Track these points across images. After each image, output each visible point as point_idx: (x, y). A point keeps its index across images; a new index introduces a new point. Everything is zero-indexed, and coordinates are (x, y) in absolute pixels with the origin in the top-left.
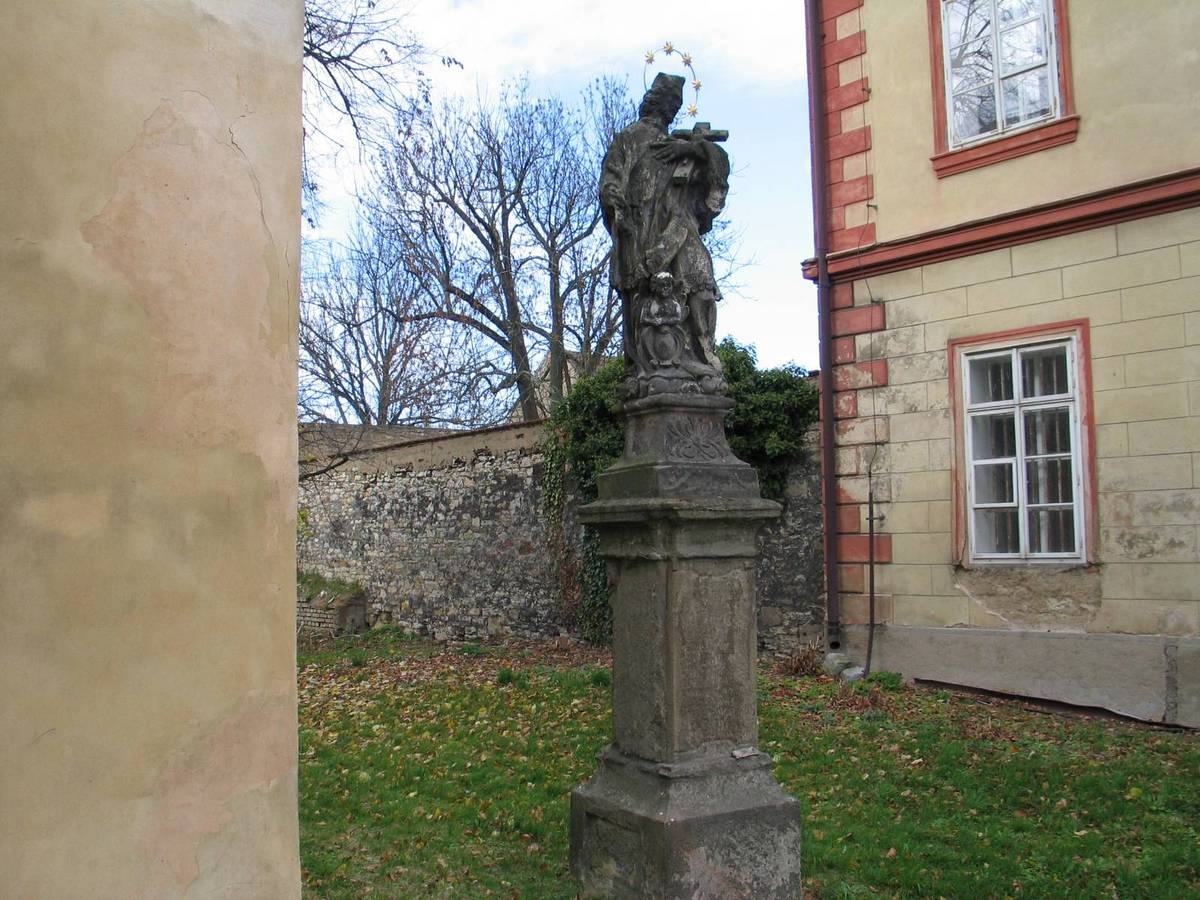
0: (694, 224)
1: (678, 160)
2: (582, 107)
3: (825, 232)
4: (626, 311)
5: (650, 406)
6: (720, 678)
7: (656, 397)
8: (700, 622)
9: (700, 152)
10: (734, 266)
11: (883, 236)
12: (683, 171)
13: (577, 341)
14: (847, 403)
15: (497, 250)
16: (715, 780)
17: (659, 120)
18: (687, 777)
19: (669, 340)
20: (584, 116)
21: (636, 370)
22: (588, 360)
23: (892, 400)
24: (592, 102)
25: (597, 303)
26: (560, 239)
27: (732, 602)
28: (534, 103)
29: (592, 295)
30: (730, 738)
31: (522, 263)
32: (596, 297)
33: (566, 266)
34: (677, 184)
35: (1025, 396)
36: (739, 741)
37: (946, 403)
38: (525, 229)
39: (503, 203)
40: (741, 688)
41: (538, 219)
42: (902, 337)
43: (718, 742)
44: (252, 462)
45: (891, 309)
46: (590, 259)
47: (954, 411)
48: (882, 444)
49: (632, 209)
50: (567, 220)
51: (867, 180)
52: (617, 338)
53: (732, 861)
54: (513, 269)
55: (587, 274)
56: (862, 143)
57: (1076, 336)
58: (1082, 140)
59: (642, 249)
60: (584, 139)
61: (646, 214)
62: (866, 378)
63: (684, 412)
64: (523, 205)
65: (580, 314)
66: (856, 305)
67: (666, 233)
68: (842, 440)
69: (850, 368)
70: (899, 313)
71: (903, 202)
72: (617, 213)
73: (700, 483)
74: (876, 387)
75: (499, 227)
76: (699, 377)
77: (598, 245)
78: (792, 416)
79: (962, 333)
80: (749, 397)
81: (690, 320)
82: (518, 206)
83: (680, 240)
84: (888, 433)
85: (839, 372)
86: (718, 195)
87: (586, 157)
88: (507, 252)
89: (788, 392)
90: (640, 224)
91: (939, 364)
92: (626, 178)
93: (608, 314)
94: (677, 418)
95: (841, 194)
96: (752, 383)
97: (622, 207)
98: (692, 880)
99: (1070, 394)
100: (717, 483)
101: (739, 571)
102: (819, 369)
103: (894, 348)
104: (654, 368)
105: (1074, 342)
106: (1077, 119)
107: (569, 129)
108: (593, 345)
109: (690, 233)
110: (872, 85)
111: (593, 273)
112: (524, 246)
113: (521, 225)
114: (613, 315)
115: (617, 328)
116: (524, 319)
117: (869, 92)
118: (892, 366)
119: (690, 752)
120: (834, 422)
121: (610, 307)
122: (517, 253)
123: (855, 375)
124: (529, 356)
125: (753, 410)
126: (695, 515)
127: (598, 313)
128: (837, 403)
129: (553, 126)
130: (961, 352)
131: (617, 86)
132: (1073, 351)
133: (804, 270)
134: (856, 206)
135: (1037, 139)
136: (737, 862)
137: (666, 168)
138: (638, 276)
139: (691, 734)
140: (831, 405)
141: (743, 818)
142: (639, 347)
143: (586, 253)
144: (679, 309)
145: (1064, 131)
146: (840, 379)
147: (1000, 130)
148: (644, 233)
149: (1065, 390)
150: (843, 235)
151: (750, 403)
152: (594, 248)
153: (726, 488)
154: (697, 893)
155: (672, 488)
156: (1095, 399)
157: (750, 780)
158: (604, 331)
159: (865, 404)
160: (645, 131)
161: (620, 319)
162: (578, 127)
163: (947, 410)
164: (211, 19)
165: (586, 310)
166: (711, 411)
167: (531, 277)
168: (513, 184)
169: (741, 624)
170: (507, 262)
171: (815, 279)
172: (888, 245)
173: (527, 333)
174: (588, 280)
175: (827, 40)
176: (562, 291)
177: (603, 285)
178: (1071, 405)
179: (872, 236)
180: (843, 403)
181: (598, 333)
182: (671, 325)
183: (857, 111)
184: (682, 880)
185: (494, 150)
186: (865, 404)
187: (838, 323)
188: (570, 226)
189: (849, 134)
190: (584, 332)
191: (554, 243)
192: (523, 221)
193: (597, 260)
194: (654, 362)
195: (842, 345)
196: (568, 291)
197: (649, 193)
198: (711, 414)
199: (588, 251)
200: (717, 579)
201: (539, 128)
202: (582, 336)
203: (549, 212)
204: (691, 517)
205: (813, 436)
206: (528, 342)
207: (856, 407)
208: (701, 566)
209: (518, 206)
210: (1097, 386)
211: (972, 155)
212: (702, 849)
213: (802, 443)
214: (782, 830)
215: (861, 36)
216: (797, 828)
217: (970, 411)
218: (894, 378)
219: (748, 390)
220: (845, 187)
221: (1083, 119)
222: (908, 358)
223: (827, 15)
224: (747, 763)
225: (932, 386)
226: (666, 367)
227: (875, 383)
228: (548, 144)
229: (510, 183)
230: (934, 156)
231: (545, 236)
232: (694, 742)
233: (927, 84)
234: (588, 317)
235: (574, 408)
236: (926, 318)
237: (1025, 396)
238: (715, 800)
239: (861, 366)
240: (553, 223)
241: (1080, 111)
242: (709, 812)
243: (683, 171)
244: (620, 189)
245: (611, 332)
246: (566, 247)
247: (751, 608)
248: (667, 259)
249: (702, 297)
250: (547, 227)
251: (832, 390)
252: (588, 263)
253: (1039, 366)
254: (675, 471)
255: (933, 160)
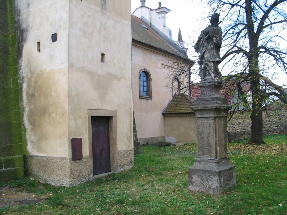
6: (206, 142)
8: (202, 130)
16: (203, 163)
18: (197, 161)
27: (209, 127)
30: (209, 155)
36: (211, 156)
40: (211, 145)
43: (206, 155)
44: (65, 109)
53: (202, 179)
63: (204, 87)
73: (202, 102)
98: (194, 181)
100: (206, 102)
101: (211, 120)
119: (201, 156)
126: (197, 109)
136: (203, 180)
139: (200, 153)
141: (205, 171)
153: (208, 102)
154: (195, 183)
155: (196, 104)
157: (211, 164)
169: (211, 131)
184: (192, 180)
198: (210, 87)
200: (206, 122)
204: (196, 109)
208: (202, 119)
212: (196, 175)
214: (214, 176)
216: (218, 177)
224: (210, 161)
232: (201, 155)
238: (202, 167)
242: (198, 168)
247: (214, 128)
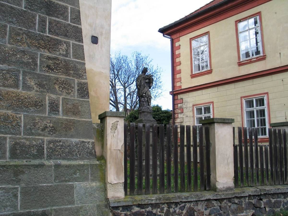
0: (148, 88)
1: (146, 79)
2: (131, 57)
3: (173, 87)
4: (139, 100)
5: (142, 112)
7: (143, 111)
9: (149, 78)
10: (163, 91)
11: (183, 87)
12: (147, 81)
13: (129, 106)
14: (177, 115)
15: (113, 87)
17: (144, 74)
19: (145, 103)
20: (132, 59)
21: (141, 107)
22: (132, 109)
23: (184, 115)
24: (133, 56)
25: (134, 98)
26: (126, 85)
28: (122, 56)
29: (133, 96)
31: (118, 90)
32: (134, 97)
33: (127, 90)
34: (146, 83)
35: (204, 114)
37: (192, 115)
38: (119, 83)
39: (115, 77)
41: (122, 80)
42: (186, 104)
45: (184, 99)
46: (132, 89)
47: (193, 116)
48: (182, 122)
49: (140, 86)
50: (128, 81)
51: (180, 78)
52: (138, 105)
54: (116, 91)
55: (132, 92)
56: (180, 72)
57: (212, 104)
58: (213, 73)
59: (141, 91)
60: (132, 64)
61: (142, 87)
62: (180, 111)
64: (119, 78)
65: (130, 100)
66: (178, 99)
67: (145, 89)
68: (176, 122)
69: (177, 110)
70: (185, 100)
71: (186, 82)
72: (138, 87)
73: (149, 122)
74: (181, 113)
75: (114, 82)
76: (149, 108)
77: (134, 87)
78: (168, 118)
79: (195, 104)
80: (160, 115)
81: (148, 101)
82: (118, 78)
83: (146, 90)
84: (183, 120)
85: (175, 110)
86: (152, 84)
87: (132, 68)
88: (115, 87)
89: (167, 114)
90: (141, 88)
91: (191, 109)
92: (139, 82)
93: (136, 101)
94: (145, 113)
95: (176, 80)
96: (161, 112)
97: (139, 86)
99: (211, 114)
102: (172, 110)
103: (184, 106)
104: (143, 107)
105: (211, 105)
106: (212, 70)
107: (129, 62)
108: (133, 107)
109: (148, 89)
110: (181, 62)
111: (133, 92)
112: (119, 86)
113: (118, 82)
114: (137, 101)
115: (138, 103)
116: (118, 101)
117: (181, 63)
118: (184, 109)
120: (174, 119)
121: (136, 99)
122: (117, 87)
123: (178, 111)
124: (119, 109)
125: (161, 117)
127: (134, 100)
128: (175, 116)
129: (125, 61)
130: (195, 107)
131: (139, 53)
132: (211, 107)
133: (170, 93)
134: (178, 82)
135: (206, 73)
137: (146, 80)
138: (141, 95)
140: (174, 116)
142: (141, 104)
143: (132, 88)
144: (146, 99)
145: (210, 72)
146: (176, 112)
147: (201, 71)
148: (142, 89)
149: (210, 113)
150: (176, 87)
151: (161, 116)
152: (133, 87)
156: (214, 114)
158: (135, 104)
159: (180, 116)
160: (142, 75)
161: (138, 102)
162: (131, 61)
163: (192, 116)
164: (102, 72)
165: (132, 100)
166: (150, 113)
167: (120, 93)
168: (117, 73)
170: (115, 89)
171: (172, 95)
172: (183, 89)
173: (119, 104)
174: (132, 93)
175: (174, 54)
176: (126, 96)
177: (135, 94)
178: (211, 115)
179: (181, 88)
180: (176, 116)
181: (134, 105)
182: (145, 101)
183: (179, 66)
185: (113, 66)
186: (180, 116)
187: (175, 102)
188: (128, 82)
189: (178, 70)
190: (131, 104)
191: (125, 85)
192: (119, 81)
193: (134, 89)
194: (143, 106)
195: (176, 106)
196: (128, 96)
197: (142, 84)
199: (132, 87)
201: (122, 61)
202: (131, 105)
203: (124, 79)
205: (171, 121)
206: (119, 106)
207: (178, 116)
209: (118, 78)
210: (215, 112)
211: (196, 75)
213: (169, 122)
215: (180, 54)
217: (196, 117)
218: (184, 111)
219: (160, 113)
220: (176, 79)
221: (213, 70)
222: (186, 108)
223: (174, 50)
225: (190, 113)
226: (144, 107)
227: (181, 112)
228: (124, 65)
229: (116, 73)
230: (191, 75)
231: (123, 84)
233: (190, 63)
234: (132, 101)
235: (130, 117)
236: (189, 101)
237: (204, 114)
239: (179, 109)
240: (125, 81)
241: (212, 68)
243: (147, 81)
244: (139, 83)
245: (137, 104)
246: (128, 86)
248: (145, 93)
249: (149, 98)
250: (123, 82)
251: (174, 113)
252: (132, 90)
253: (207, 109)
254: (145, 120)
255: (191, 75)
